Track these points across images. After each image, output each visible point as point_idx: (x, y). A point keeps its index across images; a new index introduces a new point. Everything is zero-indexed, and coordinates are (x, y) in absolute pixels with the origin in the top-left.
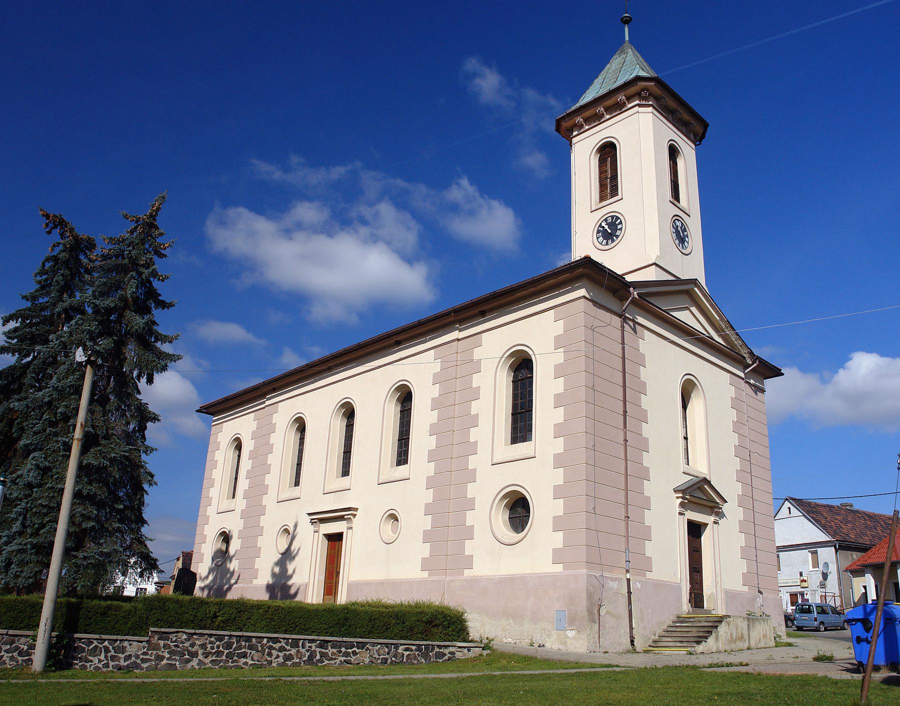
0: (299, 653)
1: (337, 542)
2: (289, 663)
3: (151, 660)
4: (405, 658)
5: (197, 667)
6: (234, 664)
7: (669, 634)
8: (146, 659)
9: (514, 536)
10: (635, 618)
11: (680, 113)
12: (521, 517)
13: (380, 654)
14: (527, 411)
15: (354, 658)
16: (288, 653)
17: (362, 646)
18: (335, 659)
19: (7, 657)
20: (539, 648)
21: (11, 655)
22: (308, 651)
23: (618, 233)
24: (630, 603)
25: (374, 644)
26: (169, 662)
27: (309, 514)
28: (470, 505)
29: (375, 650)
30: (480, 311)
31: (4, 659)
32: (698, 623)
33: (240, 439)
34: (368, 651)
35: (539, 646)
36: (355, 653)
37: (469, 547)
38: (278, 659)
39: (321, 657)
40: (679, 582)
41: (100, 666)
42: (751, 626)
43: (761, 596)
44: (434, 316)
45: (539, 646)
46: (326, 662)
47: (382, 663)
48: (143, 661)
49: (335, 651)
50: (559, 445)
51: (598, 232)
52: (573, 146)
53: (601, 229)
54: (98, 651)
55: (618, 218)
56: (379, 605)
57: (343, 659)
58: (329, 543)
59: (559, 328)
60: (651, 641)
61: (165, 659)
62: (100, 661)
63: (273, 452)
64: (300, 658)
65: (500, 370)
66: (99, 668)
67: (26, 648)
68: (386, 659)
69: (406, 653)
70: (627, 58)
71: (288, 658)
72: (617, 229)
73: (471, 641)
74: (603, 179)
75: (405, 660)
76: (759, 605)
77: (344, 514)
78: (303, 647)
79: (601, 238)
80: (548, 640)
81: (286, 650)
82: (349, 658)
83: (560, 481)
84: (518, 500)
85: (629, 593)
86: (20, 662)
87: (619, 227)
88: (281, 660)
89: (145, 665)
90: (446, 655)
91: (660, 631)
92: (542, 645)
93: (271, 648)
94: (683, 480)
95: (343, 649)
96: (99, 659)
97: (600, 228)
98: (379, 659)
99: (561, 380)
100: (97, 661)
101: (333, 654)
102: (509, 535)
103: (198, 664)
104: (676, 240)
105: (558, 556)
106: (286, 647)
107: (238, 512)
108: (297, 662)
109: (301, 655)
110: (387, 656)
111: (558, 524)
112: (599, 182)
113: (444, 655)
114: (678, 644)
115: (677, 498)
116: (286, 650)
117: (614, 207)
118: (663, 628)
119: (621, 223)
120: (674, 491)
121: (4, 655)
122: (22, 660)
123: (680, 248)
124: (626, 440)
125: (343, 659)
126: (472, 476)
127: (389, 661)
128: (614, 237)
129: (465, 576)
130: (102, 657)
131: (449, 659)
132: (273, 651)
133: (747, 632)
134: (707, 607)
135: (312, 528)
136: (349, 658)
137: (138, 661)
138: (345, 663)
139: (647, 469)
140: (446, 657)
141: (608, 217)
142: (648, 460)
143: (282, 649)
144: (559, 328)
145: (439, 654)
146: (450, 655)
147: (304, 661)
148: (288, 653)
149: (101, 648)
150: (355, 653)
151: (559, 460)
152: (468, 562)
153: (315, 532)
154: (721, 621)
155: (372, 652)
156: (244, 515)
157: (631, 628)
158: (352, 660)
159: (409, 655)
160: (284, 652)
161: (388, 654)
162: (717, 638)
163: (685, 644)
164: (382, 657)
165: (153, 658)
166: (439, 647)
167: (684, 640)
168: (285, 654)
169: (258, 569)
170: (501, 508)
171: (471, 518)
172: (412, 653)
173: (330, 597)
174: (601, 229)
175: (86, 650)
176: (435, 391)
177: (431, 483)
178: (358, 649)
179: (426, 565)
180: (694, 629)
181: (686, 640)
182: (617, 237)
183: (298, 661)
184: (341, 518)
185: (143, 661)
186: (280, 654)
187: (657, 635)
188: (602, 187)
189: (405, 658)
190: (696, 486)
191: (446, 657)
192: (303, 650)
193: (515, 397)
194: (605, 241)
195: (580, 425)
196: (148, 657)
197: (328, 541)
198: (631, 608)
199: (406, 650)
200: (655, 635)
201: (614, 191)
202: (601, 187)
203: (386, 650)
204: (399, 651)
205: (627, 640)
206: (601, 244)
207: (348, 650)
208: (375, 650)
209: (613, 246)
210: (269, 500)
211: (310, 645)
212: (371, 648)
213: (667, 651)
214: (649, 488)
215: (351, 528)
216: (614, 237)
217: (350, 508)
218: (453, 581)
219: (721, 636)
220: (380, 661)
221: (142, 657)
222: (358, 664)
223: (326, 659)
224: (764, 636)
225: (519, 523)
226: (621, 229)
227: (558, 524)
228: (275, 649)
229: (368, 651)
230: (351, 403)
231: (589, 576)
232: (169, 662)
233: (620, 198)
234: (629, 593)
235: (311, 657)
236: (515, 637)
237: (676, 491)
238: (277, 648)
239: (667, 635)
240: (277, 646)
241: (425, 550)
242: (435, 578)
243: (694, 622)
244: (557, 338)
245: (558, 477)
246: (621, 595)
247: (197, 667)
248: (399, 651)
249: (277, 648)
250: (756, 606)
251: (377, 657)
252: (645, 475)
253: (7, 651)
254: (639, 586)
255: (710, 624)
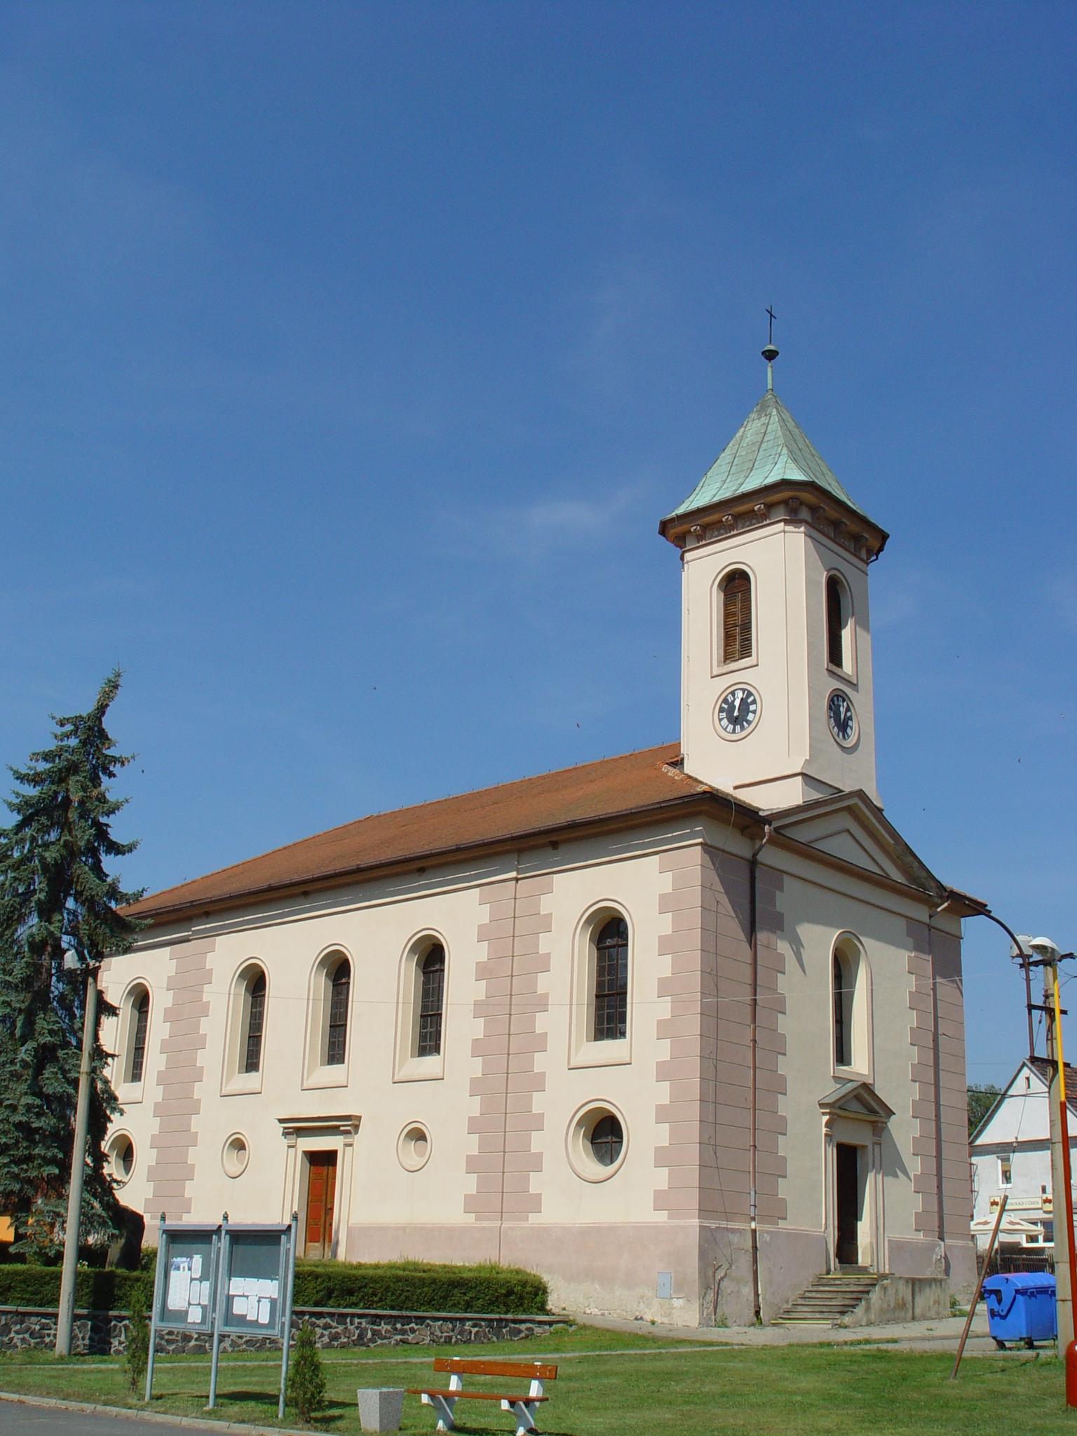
0: (347, 1331)
1: (326, 1167)
2: (336, 1343)
3: (177, 1341)
4: (473, 1335)
5: (230, 1349)
6: (271, 1345)
7: (806, 1301)
8: (171, 1339)
9: (601, 1170)
10: (761, 1281)
11: (845, 524)
12: (608, 1142)
13: (443, 1331)
14: (618, 994)
15: (412, 1336)
16: (334, 1331)
17: (420, 1320)
18: (390, 1338)
19: (18, 1339)
20: (636, 1322)
21: (21, 1336)
22: (357, 1328)
23: (751, 716)
24: (755, 1261)
25: (436, 1319)
26: (197, 1343)
27: (281, 1121)
28: (538, 1123)
29: (437, 1327)
30: (550, 842)
31: (15, 1341)
32: (845, 1286)
33: (145, 986)
34: (429, 1328)
35: (636, 1319)
36: (413, 1331)
37: (536, 1183)
38: (323, 1339)
39: (373, 1335)
40: (823, 1229)
41: (121, 1348)
42: (917, 1289)
43: (942, 1243)
44: (482, 842)
45: (636, 1319)
46: (379, 1342)
47: (445, 1342)
48: (169, 1342)
49: (389, 1327)
50: (664, 1051)
51: (721, 710)
52: (686, 565)
53: (726, 706)
54: (118, 1331)
55: (750, 694)
56: (416, 1267)
57: (398, 1337)
58: (312, 1167)
59: (665, 883)
60: (782, 1311)
61: (193, 1341)
62: (120, 1343)
63: (210, 1015)
64: (348, 1338)
65: (582, 928)
66: (120, 1351)
67: (38, 1327)
68: (451, 1338)
69: (474, 1330)
70: (770, 426)
71: (335, 1337)
72: (748, 711)
73: (553, 1314)
74: (730, 626)
75: (473, 1338)
76: (939, 1257)
77: (345, 1125)
78: (352, 1323)
79: (725, 720)
80: (647, 1311)
81: (331, 1327)
82: (406, 1337)
83: (664, 1185)
84: (608, 1117)
85: (755, 1248)
86: (32, 1345)
87: (752, 708)
88: (326, 1339)
89: (171, 1348)
90: (522, 1331)
91: (793, 1296)
92: (639, 1317)
93: (313, 1325)
94: (831, 1091)
95: (399, 1326)
96: (119, 1341)
97: (723, 705)
98: (441, 1337)
99: (665, 1171)
100: (117, 1343)
101: (387, 1331)
102: (594, 1168)
103: (231, 1346)
104: (833, 728)
105: (660, 1201)
106: (332, 1323)
107: (149, 1105)
108: (345, 1343)
109: (350, 1333)
110: (451, 1334)
111: (662, 1158)
112: (725, 629)
113: (520, 1331)
114: (818, 1316)
115: (824, 1114)
116: (331, 1327)
117: (744, 674)
118: (799, 1292)
119: (754, 702)
120: (820, 1104)
121: (14, 1337)
122: (34, 1343)
123: (840, 739)
124: (755, 1041)
125: (398, 1337)
126: (538, 1083)
127: (454, 1340)
128: (745, 723)
129: (530, 1222)
130: (123, 1338)
131: (527, 1337)
132: (317, 1329)
133: (911, 1298)
134: (863, 1262)
135: (285, 1142)
136: (406, 1337)
137: (163, 1342)
138: (401, 1343)
139: (783, 1079)
140: (523, 1335)
141: (736, 690)
142: (785, 1066)
143: (327, 1326)
144: (665, 883)
145: (514, 1330)
146: (527, 1332)
147: (353, 1341)
148: (334, 1331)
149: (120, 1328)
150: (413, 1331)
151: (663, 1072)
152: (535, 1203)
153: (289, 1147)
154: (875, 1285)
155: (433, 1329)
156: (160, 1110)
157: (757, 1295)
158: (410, 1338)
159: (477, 1332)
160: (330, 1330)
161: (453, 1330)
162: (868, 1309)
163: (826, 1315)
164: (445, 1334)
165: (179, 1338)
166: (515, 1321)
167: (824, 1310)
168: (330, 1333)
169: (191, 1198)
170: (580, 1134)
171: (537, 1142)
172: (481, 1330)
173: (316, 1244)
174: (726, 706)
175: (104, 1330)
176: (482, 952)
177: (476, 1087)
178: (417, 1325)
179: (471, 1205)
180: (840, 1295)
181: (827, 1310)
182: (749, 723)
183: (346, 1340)
184: (334, 1131)
185: (169, 1342)
186: (325, 1332)
187: (791, 1303)
188: (728, 638)
189: (473, 1335)
190: (851, 1095)
191: (523, 1335)
192: (352, 1327)
193: (601, 971)
194: (731, 727)
195: (693, 1025)
196: (174, 1337)
197: (311, 1164)
198: (757, 1268)
199: (474, 1326)
200: (787, 1302)
201: (746, 650)
202: (726, 638)
203: (450, 1326)
204: (466, 1327)
205: (750, 1310)
206: (725, 729)
207: (405, 1327)
208: (437, 1327)
209: (744, 736)
210: (205, 1091)
211: (359, 1320)
212: (431, 1323)
213: (803, 1325)
214: (785, 1106)
215: (351, 1145)
216: (745, 723)
217: (350, 1116)
218: (512, 1229)
219: (873, 1304)
220: (443, 1340)
221: (166, 1337)
222: (418, 1343)
223: (379, 1338)
224: (935, 1302)
225: (606, 1152)
226: (754, 712)
227: (662, 1158)
228: (318, 1326)
229: (429, 1328)
230: (339, 950)
231: (702, 1228)
232: (197, 1343)
233: (755, 663)
234: (755, 1248)
235: (361, 1336)
236: (601, 1308)
237: (822, 1105)
238: (321, 1325)
239: (803, 1303)
240: (321, 1322)
241: (471, 1184)
242: (486, 1224)
243: (841, 1285)
244: (663, 898)
245: (662, 1093)
246: (743, 1251)
247: (230, 1349)
248: (466, 1327)
249: (321, 1325)
250: (934, 1258)
251: (440, 1334)
252: (780, 1088)
253: (17, 1332)
254: (768, 1239)
255: (861, 1289)
